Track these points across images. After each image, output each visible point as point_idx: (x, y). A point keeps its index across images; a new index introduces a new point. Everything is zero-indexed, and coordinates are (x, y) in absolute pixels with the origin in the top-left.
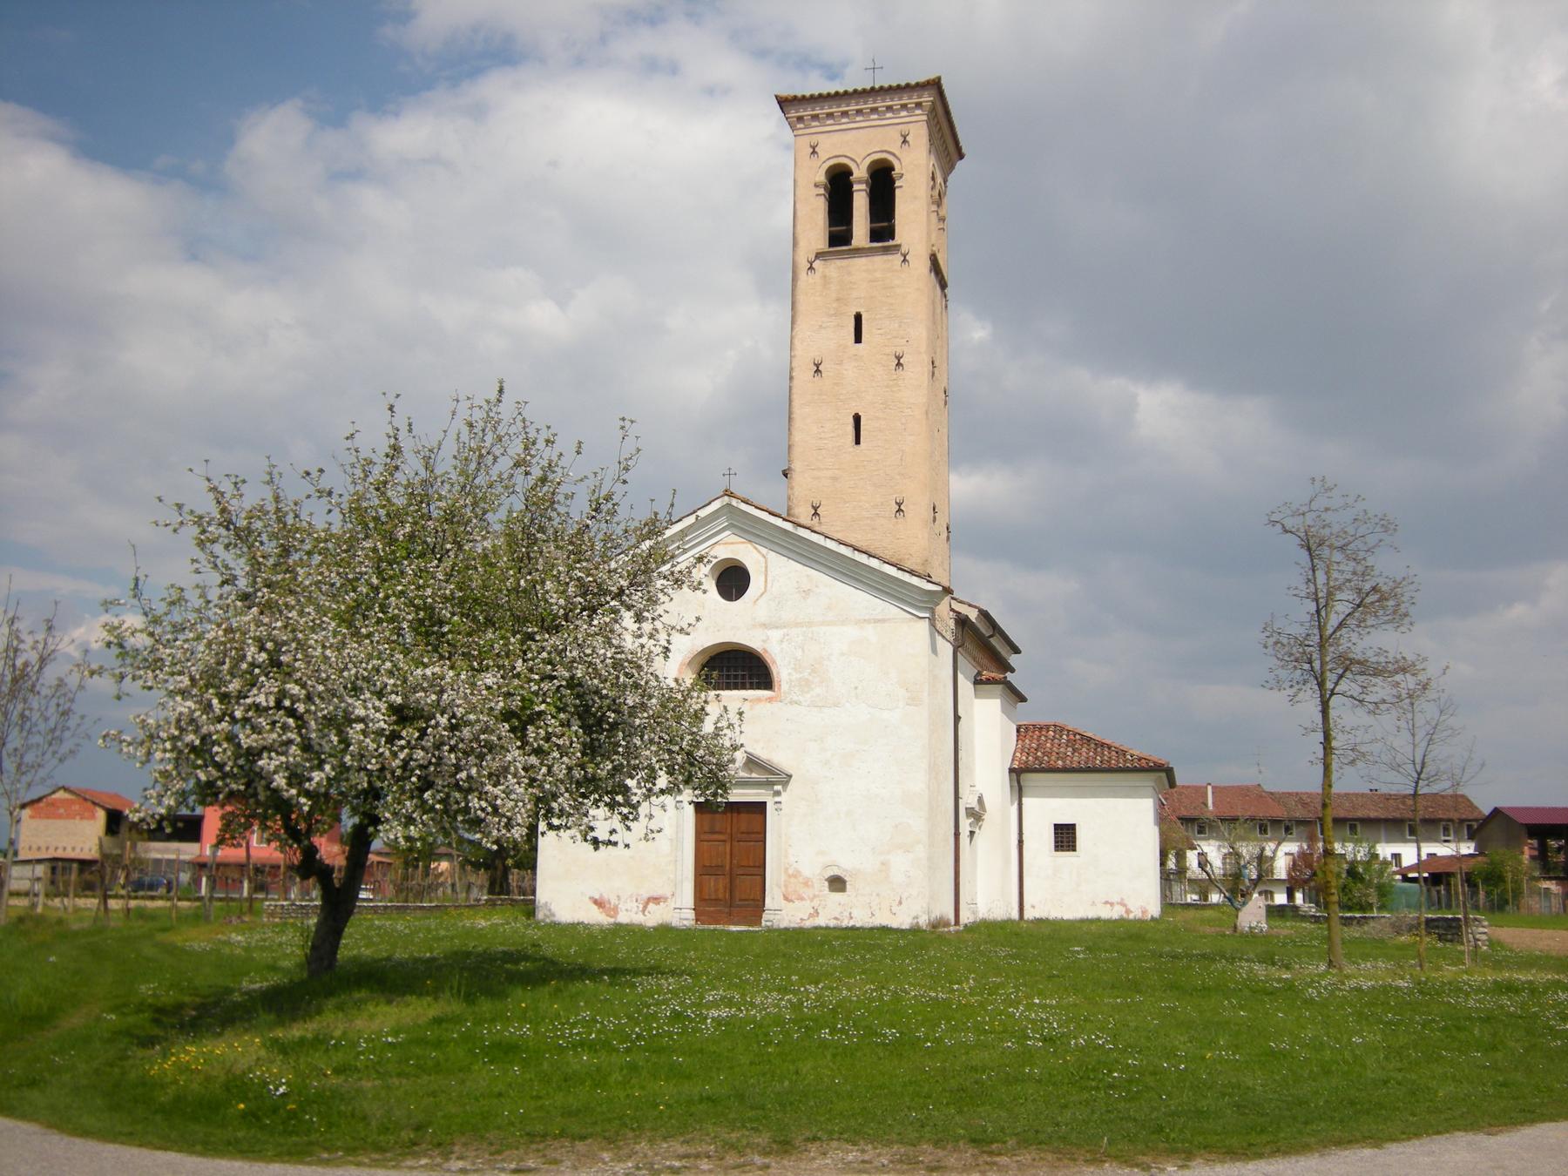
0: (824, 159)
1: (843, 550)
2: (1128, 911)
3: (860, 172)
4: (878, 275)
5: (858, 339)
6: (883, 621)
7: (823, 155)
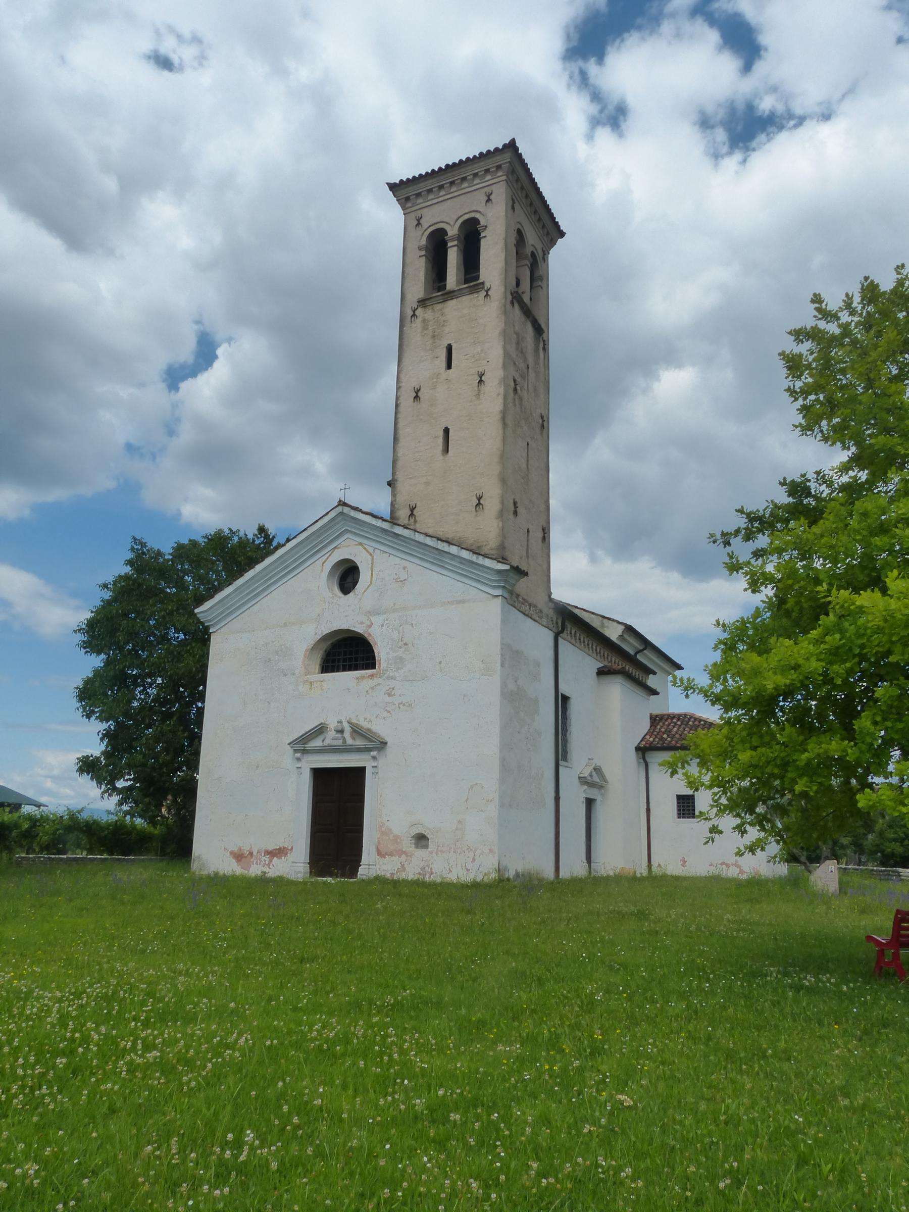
0: (426, 228)
1: (428, 541)
2: (742, 872)
3: (453, 231)
4: (465, 312)
5: (449, 366)
6: (462, 602)
7: (425, 223)
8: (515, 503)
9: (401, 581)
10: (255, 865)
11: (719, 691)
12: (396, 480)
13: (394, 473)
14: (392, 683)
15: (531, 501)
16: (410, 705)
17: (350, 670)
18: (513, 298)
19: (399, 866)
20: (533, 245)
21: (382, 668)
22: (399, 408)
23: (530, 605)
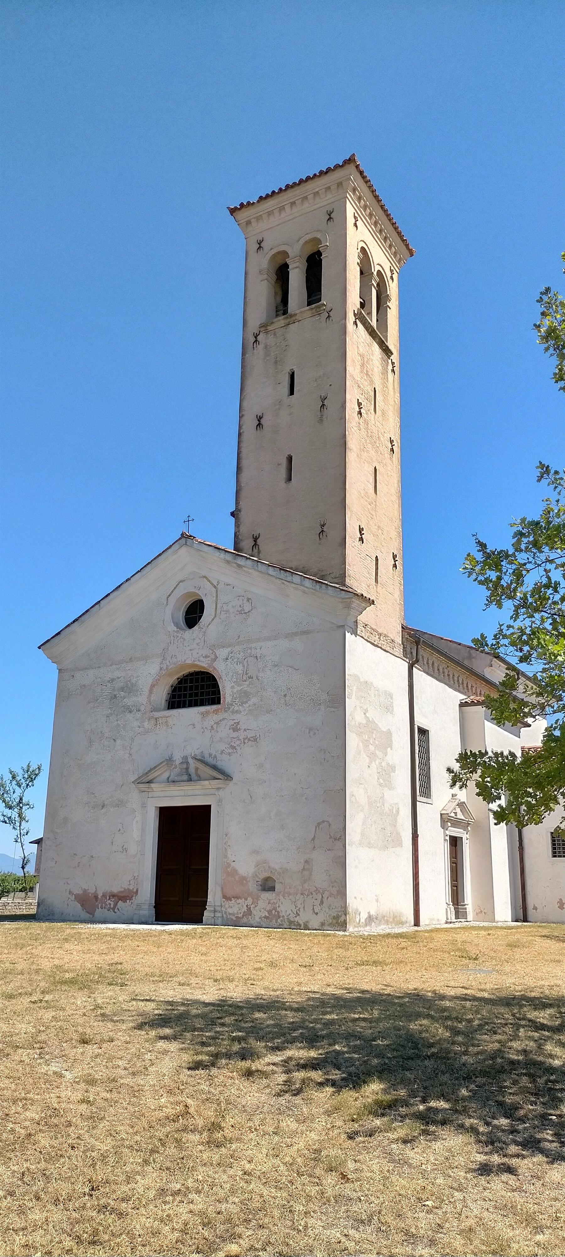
5: (292, 392)
8: (361, 530)
9: (245, 613)
10: (100, 909)
11: (520, 759)
12: (240, 511)
13: (237, 503)
14: (237, 717)
15: (379, 527)
16: (255, 740)
17: (196, 705)
18: (356, 319)
19: (245, 909)
20: (378, 264)
21: (227, 702)
22: (242, 438)
23: (380, 635)
